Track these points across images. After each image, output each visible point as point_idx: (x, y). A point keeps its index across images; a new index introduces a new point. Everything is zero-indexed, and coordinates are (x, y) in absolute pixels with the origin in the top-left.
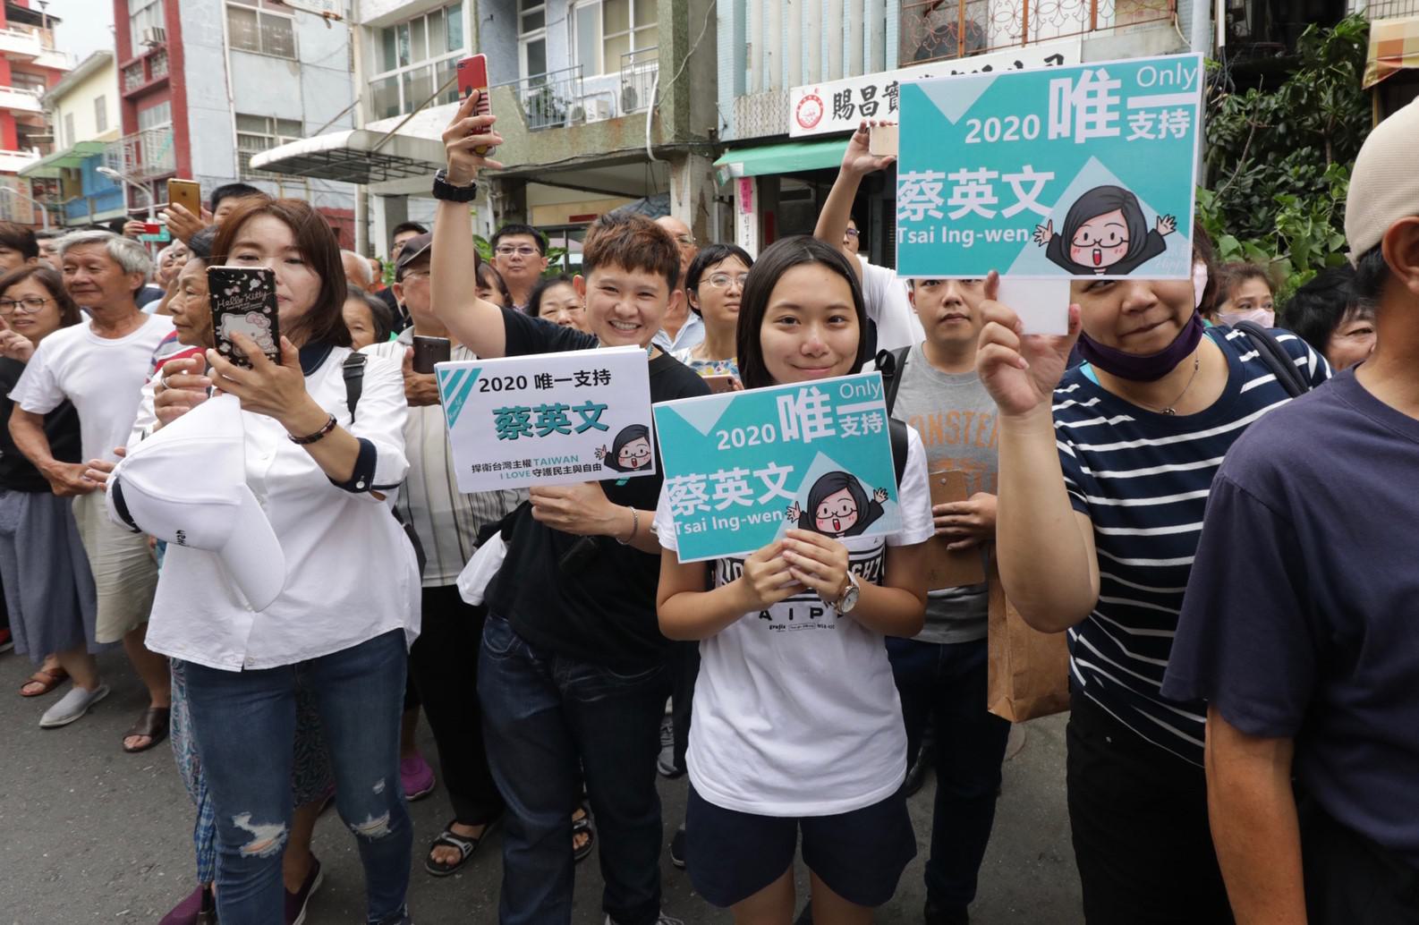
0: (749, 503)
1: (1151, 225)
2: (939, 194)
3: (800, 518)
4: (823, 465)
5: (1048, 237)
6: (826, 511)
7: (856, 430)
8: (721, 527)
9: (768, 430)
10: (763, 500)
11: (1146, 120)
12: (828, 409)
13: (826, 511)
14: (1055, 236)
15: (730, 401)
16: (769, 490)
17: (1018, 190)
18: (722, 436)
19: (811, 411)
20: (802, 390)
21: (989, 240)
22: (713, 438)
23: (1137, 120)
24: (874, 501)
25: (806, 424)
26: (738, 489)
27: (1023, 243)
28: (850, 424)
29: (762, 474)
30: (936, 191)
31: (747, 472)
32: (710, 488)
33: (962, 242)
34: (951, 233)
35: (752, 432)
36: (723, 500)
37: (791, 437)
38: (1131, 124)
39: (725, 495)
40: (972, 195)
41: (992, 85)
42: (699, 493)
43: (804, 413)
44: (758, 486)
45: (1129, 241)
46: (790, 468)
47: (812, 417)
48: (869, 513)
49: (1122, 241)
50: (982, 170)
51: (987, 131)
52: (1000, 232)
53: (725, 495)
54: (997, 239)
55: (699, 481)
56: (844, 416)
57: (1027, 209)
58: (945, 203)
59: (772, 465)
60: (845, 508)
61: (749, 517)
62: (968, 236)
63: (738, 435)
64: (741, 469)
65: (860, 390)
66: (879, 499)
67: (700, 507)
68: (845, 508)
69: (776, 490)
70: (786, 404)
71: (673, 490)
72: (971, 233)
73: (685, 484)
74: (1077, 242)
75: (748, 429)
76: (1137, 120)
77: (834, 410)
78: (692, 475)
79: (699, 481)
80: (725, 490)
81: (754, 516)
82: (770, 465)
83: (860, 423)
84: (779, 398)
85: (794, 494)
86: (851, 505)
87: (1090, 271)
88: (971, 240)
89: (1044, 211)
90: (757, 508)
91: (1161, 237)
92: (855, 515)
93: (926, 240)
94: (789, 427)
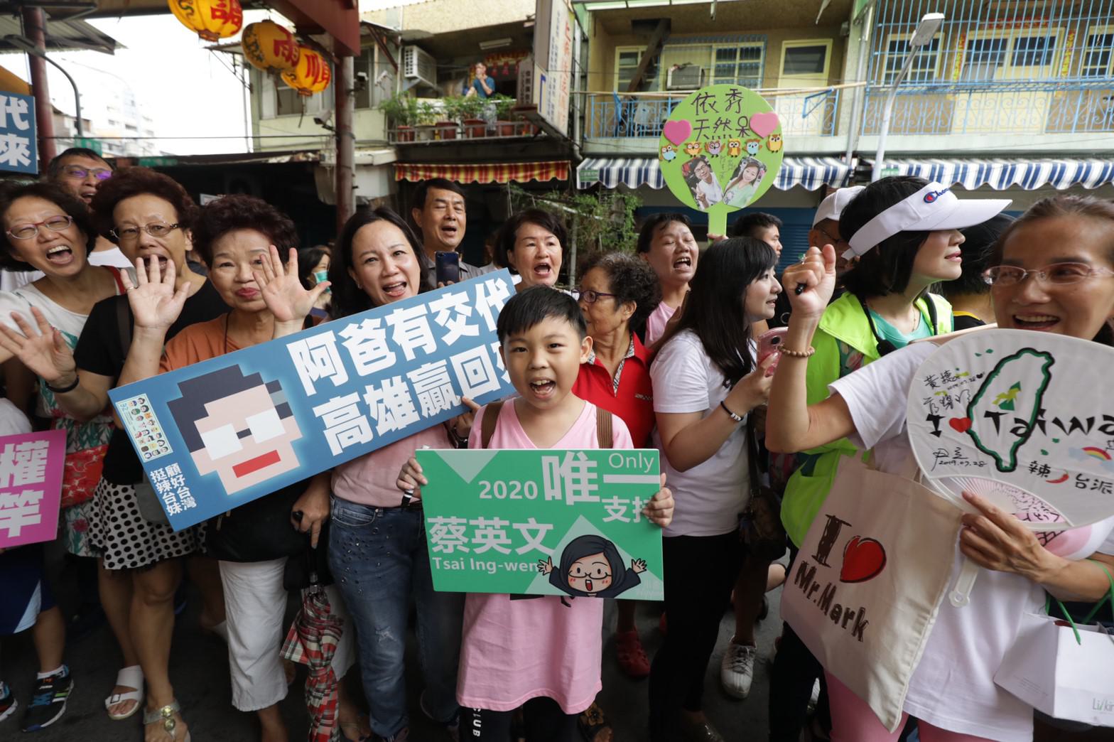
0: (507, 551)
1: (628, 565)
2: (463, 535)
6: (579, 570)
8: (478, 568)
9: (530, 486)
10: (521, 551)
11: (620, 504)
12: (594, 476)
13: (579, 570)
15: (494, 455)
16: (527, 543)
19: (576, 475)
22: (475, 487)
23: (612, 504)
25: (570, 487)
26: (497, 537)
29: (523, 528)
31: (507, 523)
32: (470, 532)
33: (487, 569)
35: (514, 486)
36: (482, 545)
37: (553, 497)
38: (606, 507)
39: (484, 541)
40: (490, 536)
42: (459, 535)
43: (569, 476)
45: (612, 576)
46: (551, 527)
47: (576, 481)
48: (621, 585)
49: (607, 575)
52: (516, 564)
53: (484, 541)
55: (458, 524)
57: (534, 549)
58: (470, 541)
59: (532, 520)
60: (599, 571)
61: (506, 564)
63: (500, 487)
64: (500, 519)
65: (631, 462)
67: (459, 548)
68: (599, 571)
69: (534, 544)
70: (551, 464)
72: (494, 564)
73: (446, 524)
74: (572, 574)
75: (511, 483)
76: (612, 504)
78: (453, 518)
79: (458, 524)
80: (485, 536)
81: (511, 564)
82: (530, 520)
86: (606, 569)
88: (494, 569)
89: (549, 552)
91: (636, 574)
92: (609, 579)
93: (458, 568)
94: (553, 488)
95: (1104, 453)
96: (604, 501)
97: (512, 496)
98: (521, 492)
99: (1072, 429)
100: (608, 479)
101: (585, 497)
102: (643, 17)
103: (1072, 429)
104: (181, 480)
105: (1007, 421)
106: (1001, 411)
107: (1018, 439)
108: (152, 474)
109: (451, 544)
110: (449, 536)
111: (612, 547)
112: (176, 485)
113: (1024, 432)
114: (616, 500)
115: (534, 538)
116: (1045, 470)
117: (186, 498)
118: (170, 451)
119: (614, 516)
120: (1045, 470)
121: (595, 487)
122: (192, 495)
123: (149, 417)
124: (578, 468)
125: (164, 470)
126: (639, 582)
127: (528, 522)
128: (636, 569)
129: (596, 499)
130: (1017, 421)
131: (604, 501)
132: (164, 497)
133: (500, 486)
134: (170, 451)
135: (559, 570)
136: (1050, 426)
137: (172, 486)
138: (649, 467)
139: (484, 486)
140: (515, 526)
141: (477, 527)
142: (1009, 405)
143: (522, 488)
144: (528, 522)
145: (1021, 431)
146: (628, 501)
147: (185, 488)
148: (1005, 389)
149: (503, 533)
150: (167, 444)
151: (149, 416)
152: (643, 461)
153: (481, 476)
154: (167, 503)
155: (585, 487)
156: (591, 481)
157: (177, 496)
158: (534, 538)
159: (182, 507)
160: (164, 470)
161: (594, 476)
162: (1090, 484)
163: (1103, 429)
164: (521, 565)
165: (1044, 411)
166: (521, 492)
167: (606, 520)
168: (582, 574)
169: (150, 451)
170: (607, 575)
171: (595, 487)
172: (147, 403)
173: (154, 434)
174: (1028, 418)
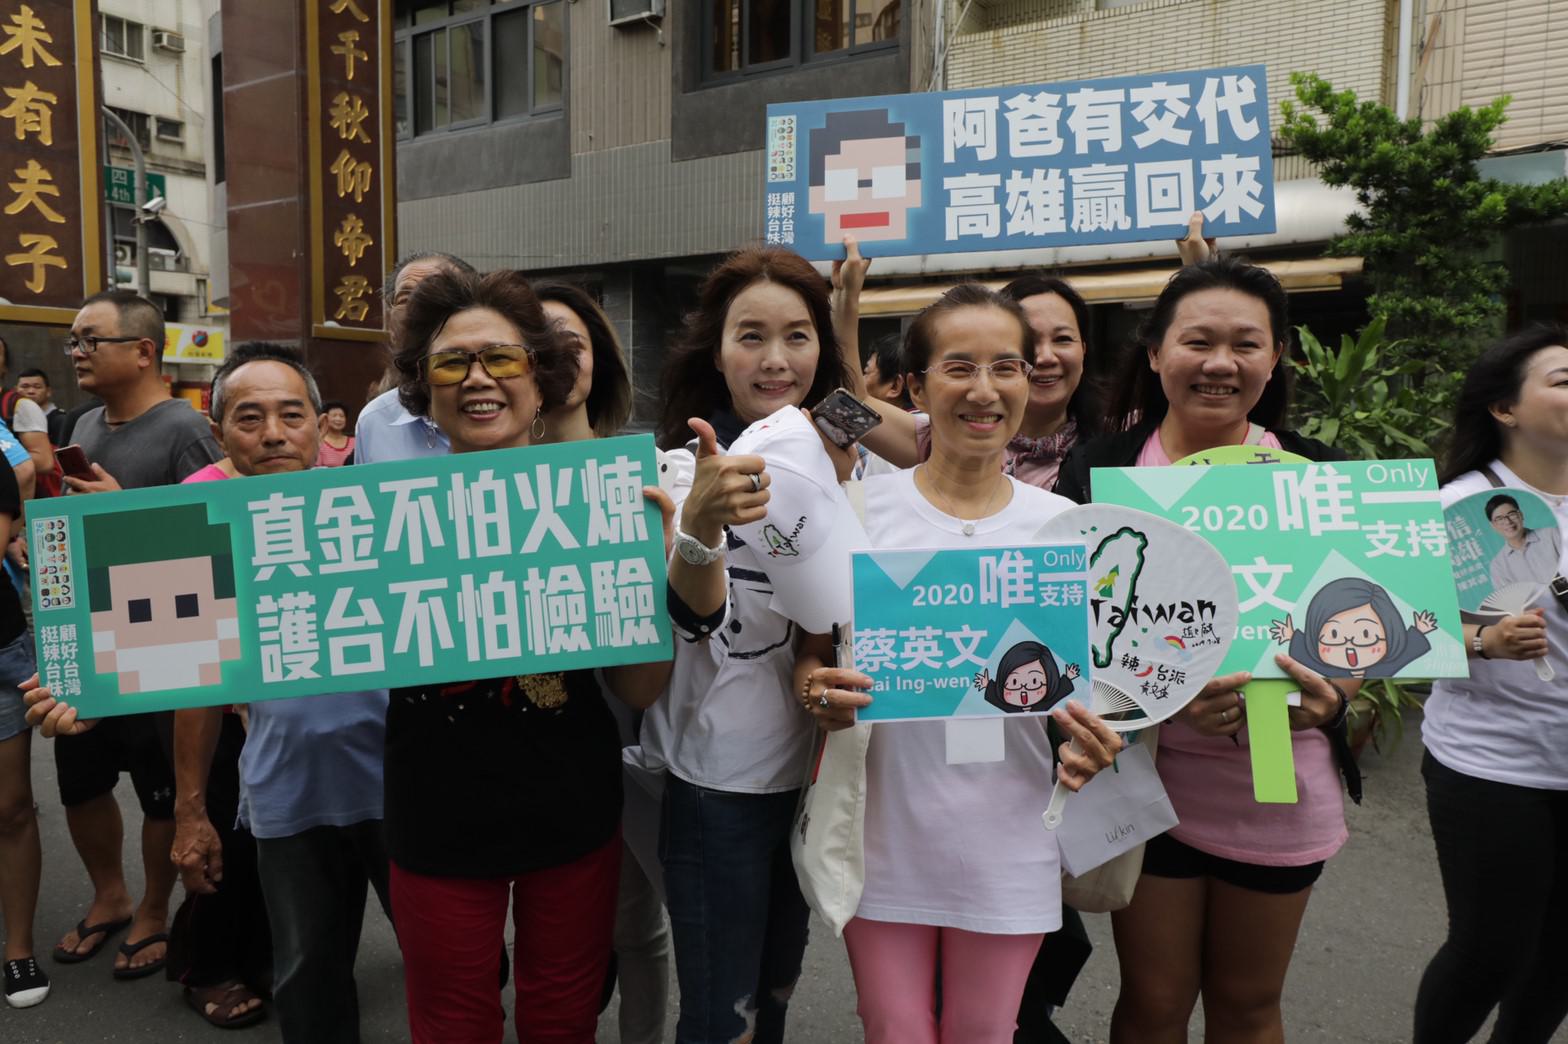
1: (1409, 622)
2: (892, 649)
3: (987, 688)
4: (1018, 633)
5: (985, 683)
6: (1334, 634)
7: (1056, 600)
10: (952, 663)
11: (1388, 532)
12: (1348, 494)
13: (1334, 634)
14: (991, 682)
17: (959, 646)
18: (919, 591)
19: (1322, 495)
20: (1006, 552)
21: (937, 686)
23: (1376, 532)
24: (1065, 676)
25: (1314, 512)
26: (928, 649)
27: (966, 689)
28: (1050, 593)
30: (889, 646)
31: (939, 632)
32: (899, 646)
33: (914, 689)
34: (904, 682)
37: (1291, 526)
38: (1368, 536)
40: (921, 648)
41: (922, 571)
44: (949, 649)
45: (1386, 639)
46: (1289, 569)
47: (1012, 582)
49: (1378, 639)
50: (929, 628)
51: (930, 596)
54: (944, 686)
55: (888, 637)
56: (1045, 584)
58: (898, 656)
59: (1260, 561)
60: (1366, 634)
62: (919, 684)
66: (1070, 675)
67: (885, 664)
68: (1366, 634)
69: (967, 654)
70: (1286, 482)
71: (860, 644)
73: (873, 638)
74: (1324, 640)
75: (1229, 509)
76: (1376, 532)
77: (1036, 577)
79: (888, 637)
83: (1060, 593)
84: (981, 559)
85: (985, 661)
86: (1377, 630)
87: (1019, 709)
88: (922, 687)
89: (1287, 606)
90: (945, 672)
92: (1382, 645)
94: (989, 590)
95: (1180, 641)
96: (1365, 528)
97: (1231, 526)
98: (1244, 521)
99: (1158, 617)
100: (1368, 498)
101: (1338, 524)
102: (350, 338)
103: (1158, 617)
104: (791, 211)
105: (1106, 612)
106: (1101, 599)
107: (1114, 629)
108: (43, 631)
109: (876, 661)
110: (876, 652)
111: (1384, 596)
112: (785, 215)
113: (1120, 620)
114: (1381, 526)
115: (1254, 595)
116: (1135, 663)
117: (71, 678)
118: (793, 178)
119: (1381, 549)
120: (1135, 663)
121: (1351, 510)
122: (79, 677)
123: (63, 549)
124: (1325, 485)
125: (58, 629)
126: (1427, 647)
127: (1254, 563)
128: (1422, 628)
129: (1354, 526)
130: (1115, 609)
131: (1365, 528)
132: (48, 668)
133: (1212, 513)
134: (793, 178)
135: (1304, 635)
136: (1141, 614)
137: (61, 655)
138: (1423, 480)
139: (1190, 514)
140: (948, 635)
141: (907, 639)
142: (1107, 592)
143: (1246, 516)
144: (1254, 563)
145: (1117, 621)
146: (1399, 527)
147: (75, 665)
148: (1105, 574)
149: (934, 644)
150: (793, 171)
151: (62, 548)
152: (1414, 473)
153: (1186, 499)
154: (49, 677)
155: (1336, 510)
156: (1027, 581)
157: (781, 226)
158: (1254, 595)
159: (64, 690)
160: (58, 629)
161: (1030, 575)
162: (1168, 675)
163: (1181, 616)
164: (1244, 629)
165: (1137, 597)
166: (1244, 521)
167: (1370, 554)
168: (1340, 639)
169: (50, 597)
170: (1378, 639)
171: (1351, 510)
172: (794, 125)
173: (787, 157)
174: (1123, 608)
